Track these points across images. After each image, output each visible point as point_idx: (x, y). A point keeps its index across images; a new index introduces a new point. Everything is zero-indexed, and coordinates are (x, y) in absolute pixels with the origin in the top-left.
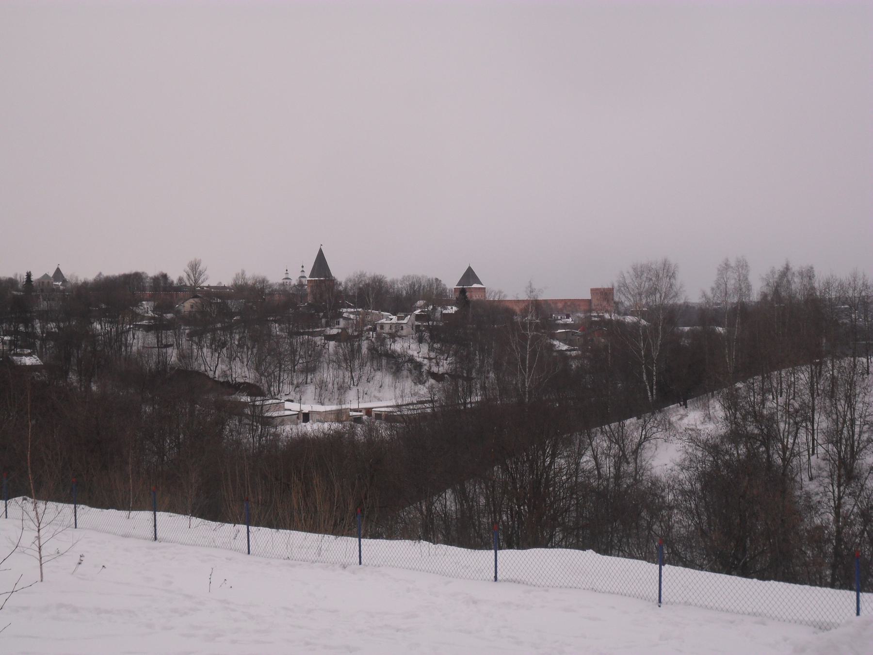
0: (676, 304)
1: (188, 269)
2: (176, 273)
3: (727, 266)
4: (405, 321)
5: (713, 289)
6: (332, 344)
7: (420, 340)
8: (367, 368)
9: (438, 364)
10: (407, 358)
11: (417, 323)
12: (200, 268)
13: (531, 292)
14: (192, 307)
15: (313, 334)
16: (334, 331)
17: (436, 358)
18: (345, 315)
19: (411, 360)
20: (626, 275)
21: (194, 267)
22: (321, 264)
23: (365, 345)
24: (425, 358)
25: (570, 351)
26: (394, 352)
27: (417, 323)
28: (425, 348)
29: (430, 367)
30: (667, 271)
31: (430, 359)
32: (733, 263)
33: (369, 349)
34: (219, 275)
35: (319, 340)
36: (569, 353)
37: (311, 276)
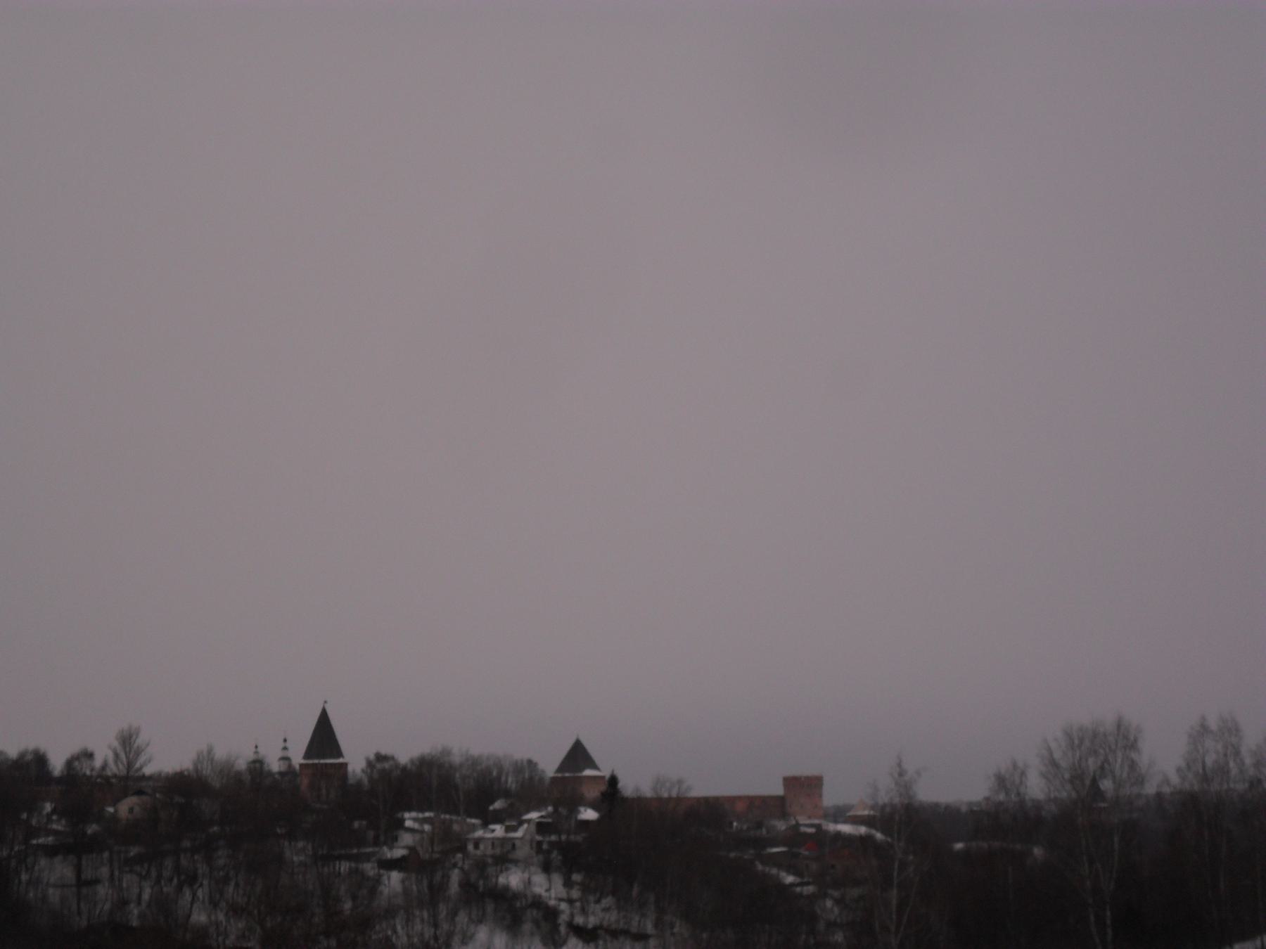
0: (1139, 796)
1: (116, 744)
2: (104, 753)
3: (1204, 729)
4: (519, 834)
5: (1179, 770)
6: (395, 877)
7: (547, 868)
8: (462, 918)
9: (584, 911)
10: (530, 900)
11: (539, 838)
12: (139, 741)
13: (901, 774)
14: (131, 810)
15: (358, 858)
16: (399, 853)
17: (580, 900)
18: (408, 823)
19: (537, 903)
20: (1053, 745)
21: (127, 740)
22: (324, 737)
23: (455, 876)
24: (561, 900)
25: (801, 884)
26: (507, 888)
27: (539, 838)
28: (558, 880)
29: (572, 915)
30: (1124, 738)
31: (570, 901)
32: (1213, 724)
33: (461, 885)
34: (166, 756)
35: (370, 868)
36: (798, 889)
37: (308, 755)
